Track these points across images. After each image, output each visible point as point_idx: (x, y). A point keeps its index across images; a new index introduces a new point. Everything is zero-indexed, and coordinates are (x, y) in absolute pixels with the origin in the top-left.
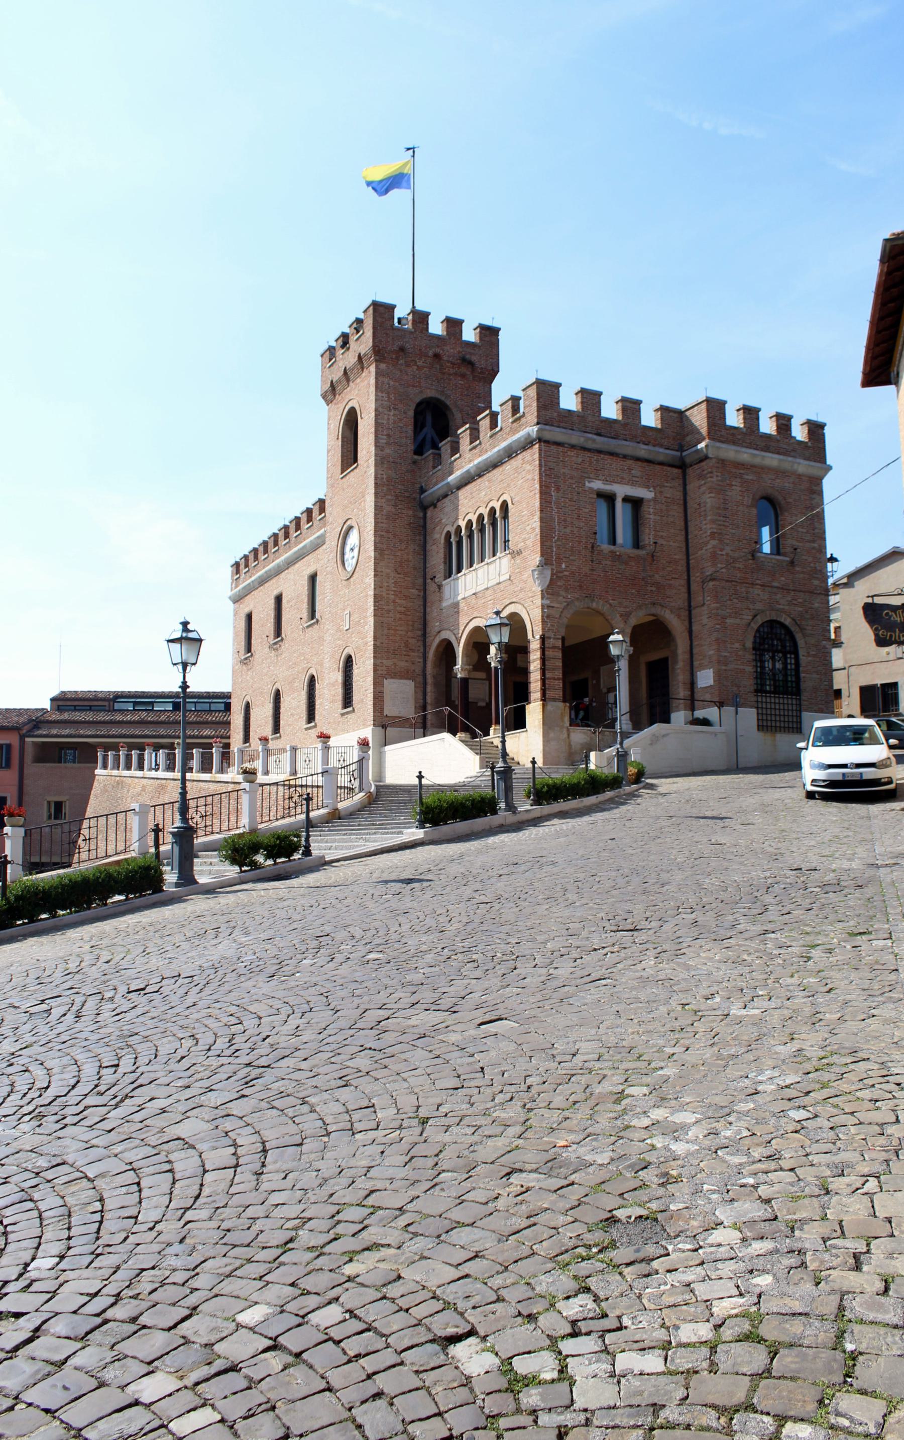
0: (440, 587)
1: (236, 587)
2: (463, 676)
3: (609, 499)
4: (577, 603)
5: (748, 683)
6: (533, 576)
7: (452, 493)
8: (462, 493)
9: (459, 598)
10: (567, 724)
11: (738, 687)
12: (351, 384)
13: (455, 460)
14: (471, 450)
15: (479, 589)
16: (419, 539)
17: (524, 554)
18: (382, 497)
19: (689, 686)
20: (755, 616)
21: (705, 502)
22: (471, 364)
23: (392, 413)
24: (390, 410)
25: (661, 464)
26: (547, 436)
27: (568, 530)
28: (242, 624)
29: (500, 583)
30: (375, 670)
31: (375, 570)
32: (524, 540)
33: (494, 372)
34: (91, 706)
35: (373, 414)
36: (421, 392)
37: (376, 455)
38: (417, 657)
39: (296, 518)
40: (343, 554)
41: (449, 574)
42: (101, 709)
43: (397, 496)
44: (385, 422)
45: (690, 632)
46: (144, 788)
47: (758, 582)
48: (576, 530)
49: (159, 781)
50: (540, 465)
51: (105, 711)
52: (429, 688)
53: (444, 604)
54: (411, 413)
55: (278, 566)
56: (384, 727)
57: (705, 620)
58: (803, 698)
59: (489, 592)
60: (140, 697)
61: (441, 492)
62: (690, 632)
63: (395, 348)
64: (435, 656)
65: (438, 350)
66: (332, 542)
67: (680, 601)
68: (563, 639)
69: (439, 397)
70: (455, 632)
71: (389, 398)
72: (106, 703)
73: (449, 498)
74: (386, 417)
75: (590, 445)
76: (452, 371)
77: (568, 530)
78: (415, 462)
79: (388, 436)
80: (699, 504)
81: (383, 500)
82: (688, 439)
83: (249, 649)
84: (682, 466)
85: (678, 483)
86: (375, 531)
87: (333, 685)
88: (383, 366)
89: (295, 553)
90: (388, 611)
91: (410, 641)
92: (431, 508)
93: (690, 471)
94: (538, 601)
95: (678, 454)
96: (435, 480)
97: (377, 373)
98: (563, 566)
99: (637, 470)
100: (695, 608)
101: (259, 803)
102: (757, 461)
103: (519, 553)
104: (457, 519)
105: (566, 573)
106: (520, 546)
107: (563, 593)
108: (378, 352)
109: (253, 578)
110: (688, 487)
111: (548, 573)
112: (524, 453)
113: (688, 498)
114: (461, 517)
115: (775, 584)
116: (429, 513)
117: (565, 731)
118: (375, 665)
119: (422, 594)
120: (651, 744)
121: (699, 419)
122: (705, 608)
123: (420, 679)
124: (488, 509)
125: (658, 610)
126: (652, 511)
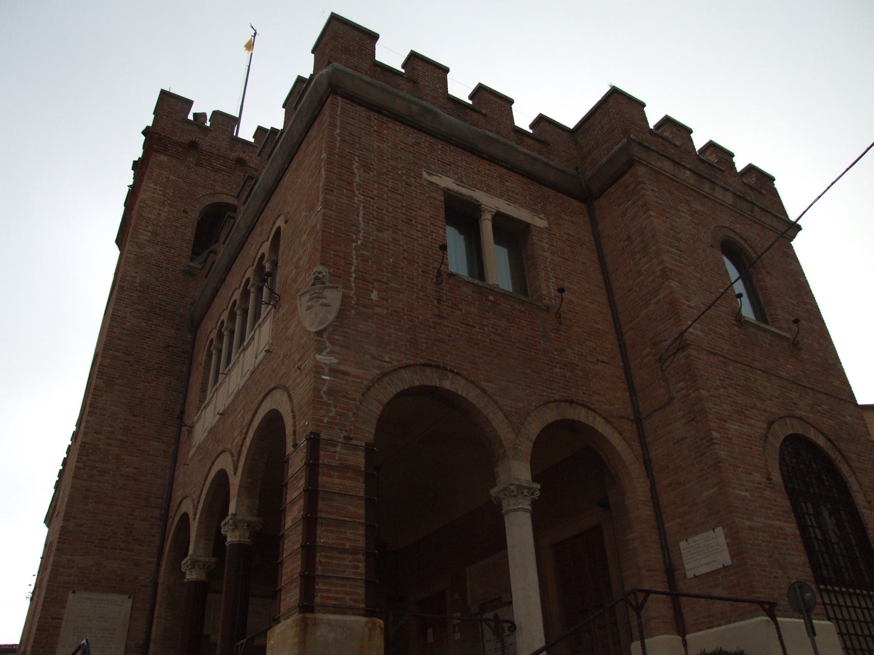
5: (798, 566)
20: (770, 424)
23: (166, 210)
27: (386, 236)
44: (153, 217)
45: (647, 463)
74: (155, 212)
79: (155, 234)
80: (629, 238)
98: (374, 296)
105: (379, 310)
126: (546, 246)
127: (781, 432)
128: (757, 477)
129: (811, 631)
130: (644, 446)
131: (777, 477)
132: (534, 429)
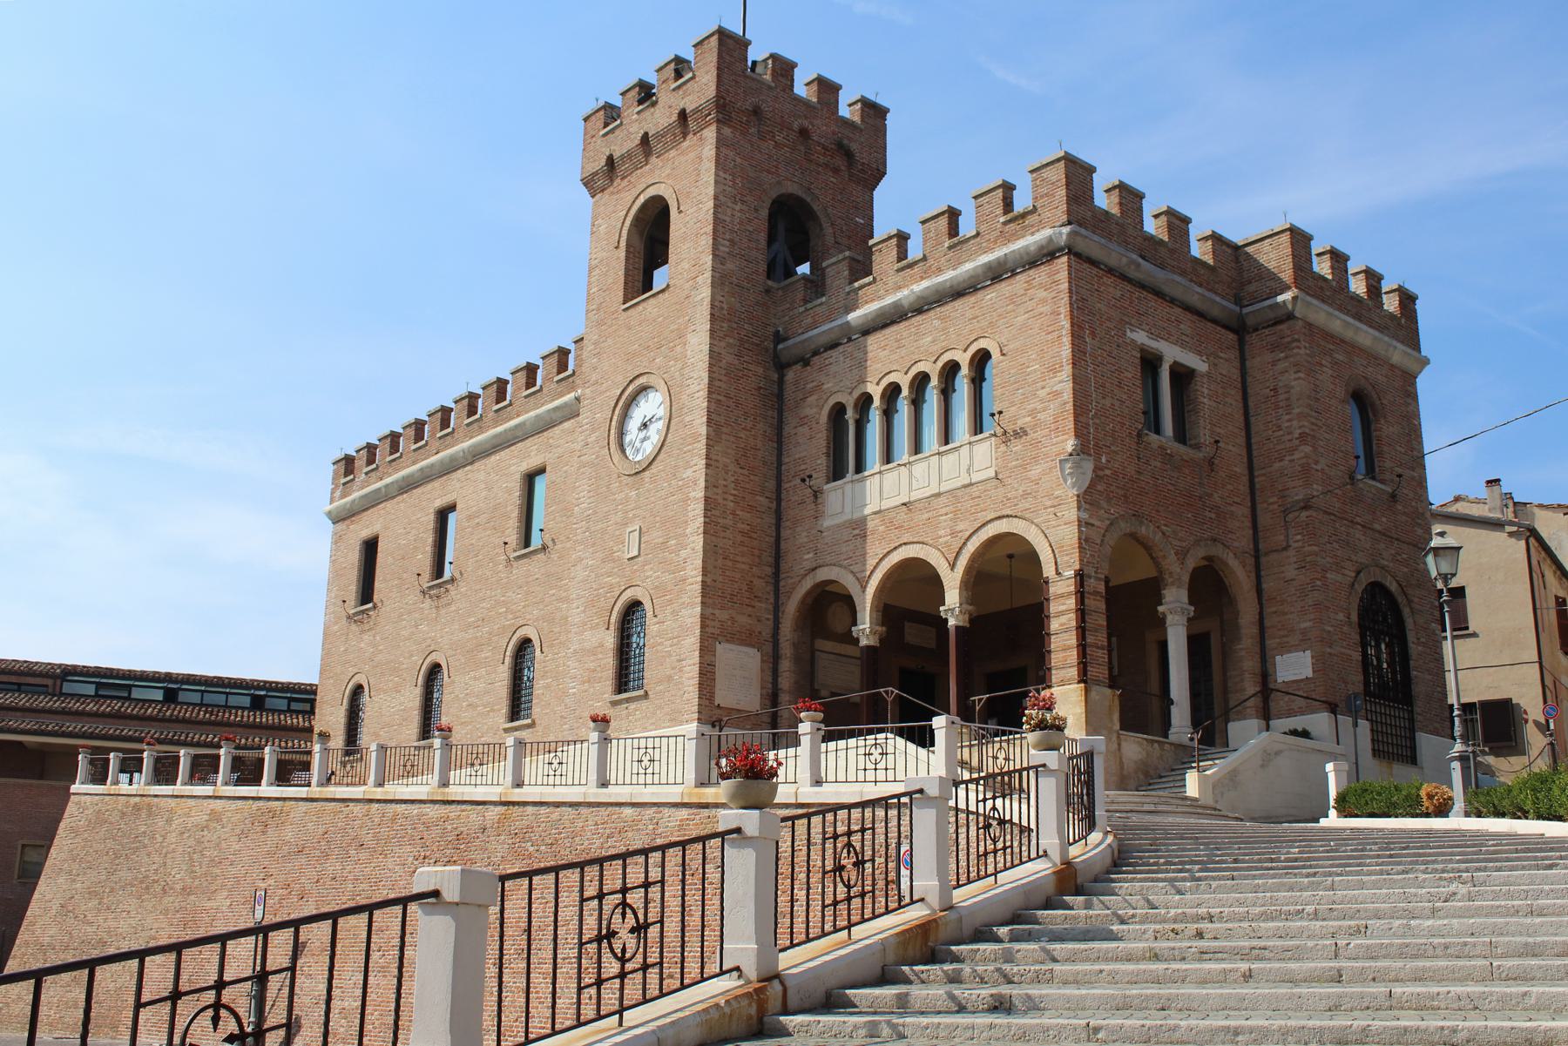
0: (816, 494)
1: (343, 496)
2: (872, 643)
3: (1150, 363)
4: (1123, 525)
5: (1356, 681)
6: (1062, 470)
7: (850, 340)
8: (873, 341)
9: (867, 511)
10: (1117, 726)
11: (1346, 683)
12: (653, 159)
13: (861, 288)
14: (899, 270)
15: (915, 495)
16: (784, 409)
17: (1032, 435)
18: (722, 339)
19: (1259, 679)
20: (1358, 573)
21: (1288, 388)
22: (848, 155)
24: (735, 203)
25: (1214, 321)
26: (1081, 246)
27: (1108, 402)
28: (354, 557)
29: (971, 484)
30: (703, 626)
31: (708, 457)
32: (1033, 413)
33: (878, 173)
34: (19, 685)
35: (711, 204)
36: (779, 183)
37: (714, 269)
38: (764, 608)
39: (499, 380)
40: (621, 434)
41: (837, 473)
42: (41, 690)
43: (741, 340)
45: (1259, 591)
46: (215, 816)
47: (1358, 520)
48: (1117, 403)
49: (261, 803)
50: (1070, 291)
51: (46, 694)
52: (786, 665)
53: (827, 523)
54: (765, 213)
55: (453, 458)
56: (716, 723)
57: (1290, 572)
58: (1417, 709)
59: (943, 499)
60: (105, 676)
61: (824, 340)
62: (1259, 591)
63: (748, 106)
64: (799, 610)
65: (806, 123)
66: (597, 411)
67: (1243, 540)
68: (1107, 581)
69: (800, 193)
70: (855, 568)
71: (733, 181)
72: (49, 682)
73: (841, 349)
74: (729, 212)
75: (1133, 274)
76: (822, 160)
77: (1108, 402)
78: (768, 291)
80: (1275, 390)
81: (723, 344)
82: (1252, 288)
83: (366, 592)
84: (1240, 329)
85: (1233, 355)
86: (710, 392)
87: (593, 652)
88: (727, 131)
89: (496, 436)
90: (725, 528)
91: (757, 582)
92: (798, 366)
93: (1252, 339)
94: (1071, 513)
95: (1237, 309)
96: (809, 320)
97: (718, 140)
99: (1187, 324)
100: (1266, 554)
101: (952, 829)
102: (1349, 334)
103: (1020, 433)
104: (863, 381)
105: (1108, 472)
106: (1020, 423)
107: (1104, 504)
108: (722, 108)
109: (388, 480)
110: (1248, 364)
111: (1089, 466)
112: (1031, 272)
113: (1249, 379)
114: (872, 377)
115: (1377, 527)
116: (790, 375)
117: (1114, 738)
118: (703, 617)
119: (774, 505)
120: (1262, 766)
121: (1277, 258)
122: (1291, 552)
123: (768, 648)
124: (940, 364)
125: (1217, 551)
127: (1364, 580)
128: (1341, 616)
129: (1356, 725)
130: (1258, 577)
131: (1354, 617)
132: (1191, 564)
